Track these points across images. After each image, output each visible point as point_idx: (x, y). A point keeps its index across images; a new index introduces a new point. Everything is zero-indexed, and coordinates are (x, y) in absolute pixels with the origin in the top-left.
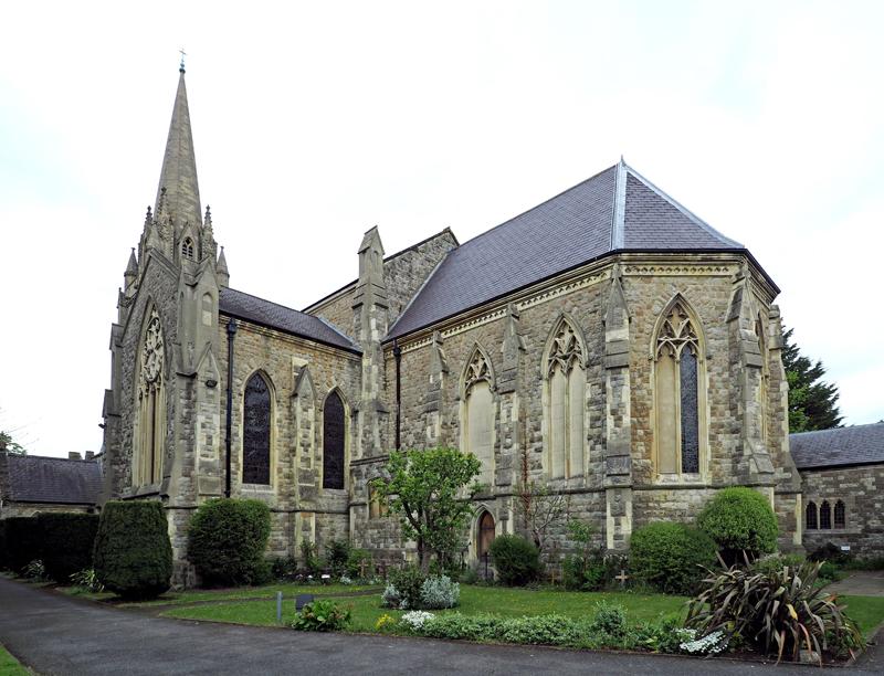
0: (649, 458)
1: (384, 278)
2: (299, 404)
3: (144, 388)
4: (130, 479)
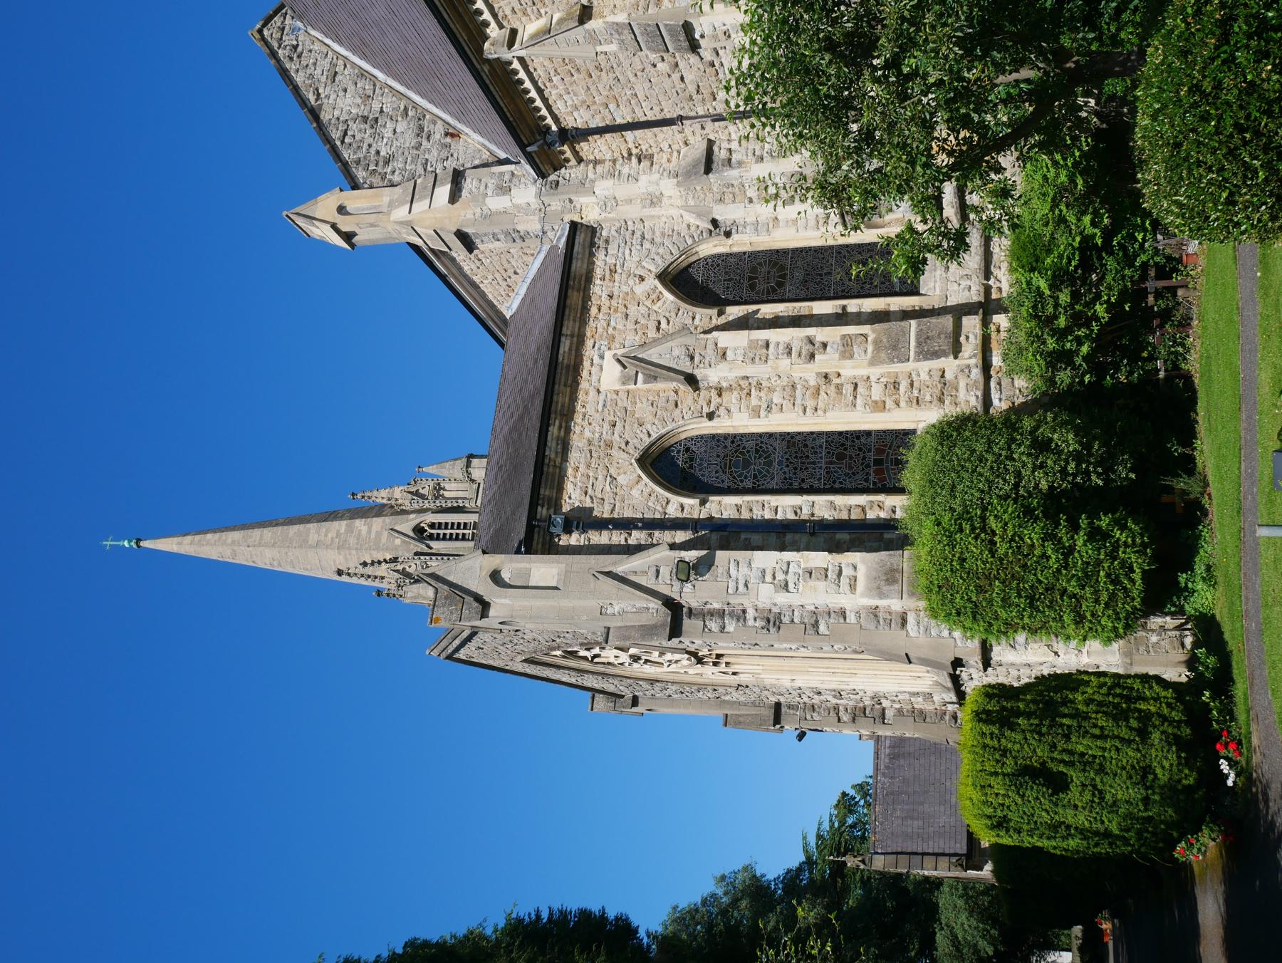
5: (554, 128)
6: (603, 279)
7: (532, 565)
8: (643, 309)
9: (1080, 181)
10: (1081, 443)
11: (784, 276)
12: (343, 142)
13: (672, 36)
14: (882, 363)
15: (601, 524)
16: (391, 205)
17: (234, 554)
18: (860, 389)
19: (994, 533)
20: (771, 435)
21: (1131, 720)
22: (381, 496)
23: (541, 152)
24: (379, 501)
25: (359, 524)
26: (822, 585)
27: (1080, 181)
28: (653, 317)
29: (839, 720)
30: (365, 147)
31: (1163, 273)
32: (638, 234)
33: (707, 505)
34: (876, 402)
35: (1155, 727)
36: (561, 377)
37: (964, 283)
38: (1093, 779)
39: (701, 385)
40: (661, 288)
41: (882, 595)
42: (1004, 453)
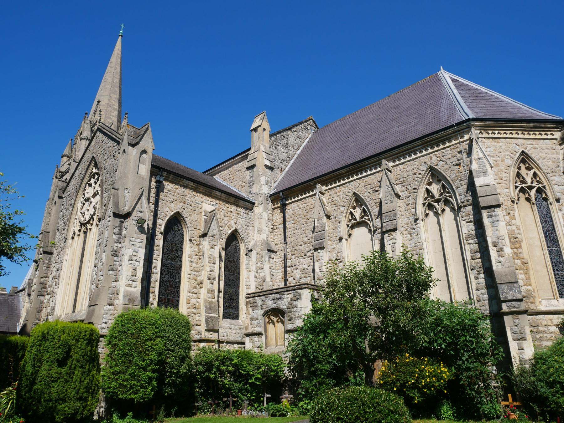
0: (530, 285)
1: (270, 147)
2: (207, 242)
3: (78, 228)
4: (53, 309)
5: (287, 202)
6: (237, 210)
8: (226, 222)
9: (272, 374)
10: (182, 375)
11: (231, 272)
12: (282, 135)
13: (320, 243)
14: (205, 303)
15: (158, 194)
16: (264, 146)
17: (111, 67)
18: (195, 295)
19: (154, 340)
20: (181, 261)
21: (86, 394)
22: (124, 123)
23: (279, 197)
24: (123, 122)
25: (116, 113)
26: (130, 274)
27: (272, 374)
28: (224, 225)
29: (42, 277)
30: (280, 142)
31: (234, 403)
32: (249, 224)
33: (160, 235)
34: (190, 300)
35: (82, 404)
36: (208, 190)
37: (225, 334)
38: (63, 378)
39: (202, 239)
40: (233, 229)
41: (124, 296)
42: (182, 345)
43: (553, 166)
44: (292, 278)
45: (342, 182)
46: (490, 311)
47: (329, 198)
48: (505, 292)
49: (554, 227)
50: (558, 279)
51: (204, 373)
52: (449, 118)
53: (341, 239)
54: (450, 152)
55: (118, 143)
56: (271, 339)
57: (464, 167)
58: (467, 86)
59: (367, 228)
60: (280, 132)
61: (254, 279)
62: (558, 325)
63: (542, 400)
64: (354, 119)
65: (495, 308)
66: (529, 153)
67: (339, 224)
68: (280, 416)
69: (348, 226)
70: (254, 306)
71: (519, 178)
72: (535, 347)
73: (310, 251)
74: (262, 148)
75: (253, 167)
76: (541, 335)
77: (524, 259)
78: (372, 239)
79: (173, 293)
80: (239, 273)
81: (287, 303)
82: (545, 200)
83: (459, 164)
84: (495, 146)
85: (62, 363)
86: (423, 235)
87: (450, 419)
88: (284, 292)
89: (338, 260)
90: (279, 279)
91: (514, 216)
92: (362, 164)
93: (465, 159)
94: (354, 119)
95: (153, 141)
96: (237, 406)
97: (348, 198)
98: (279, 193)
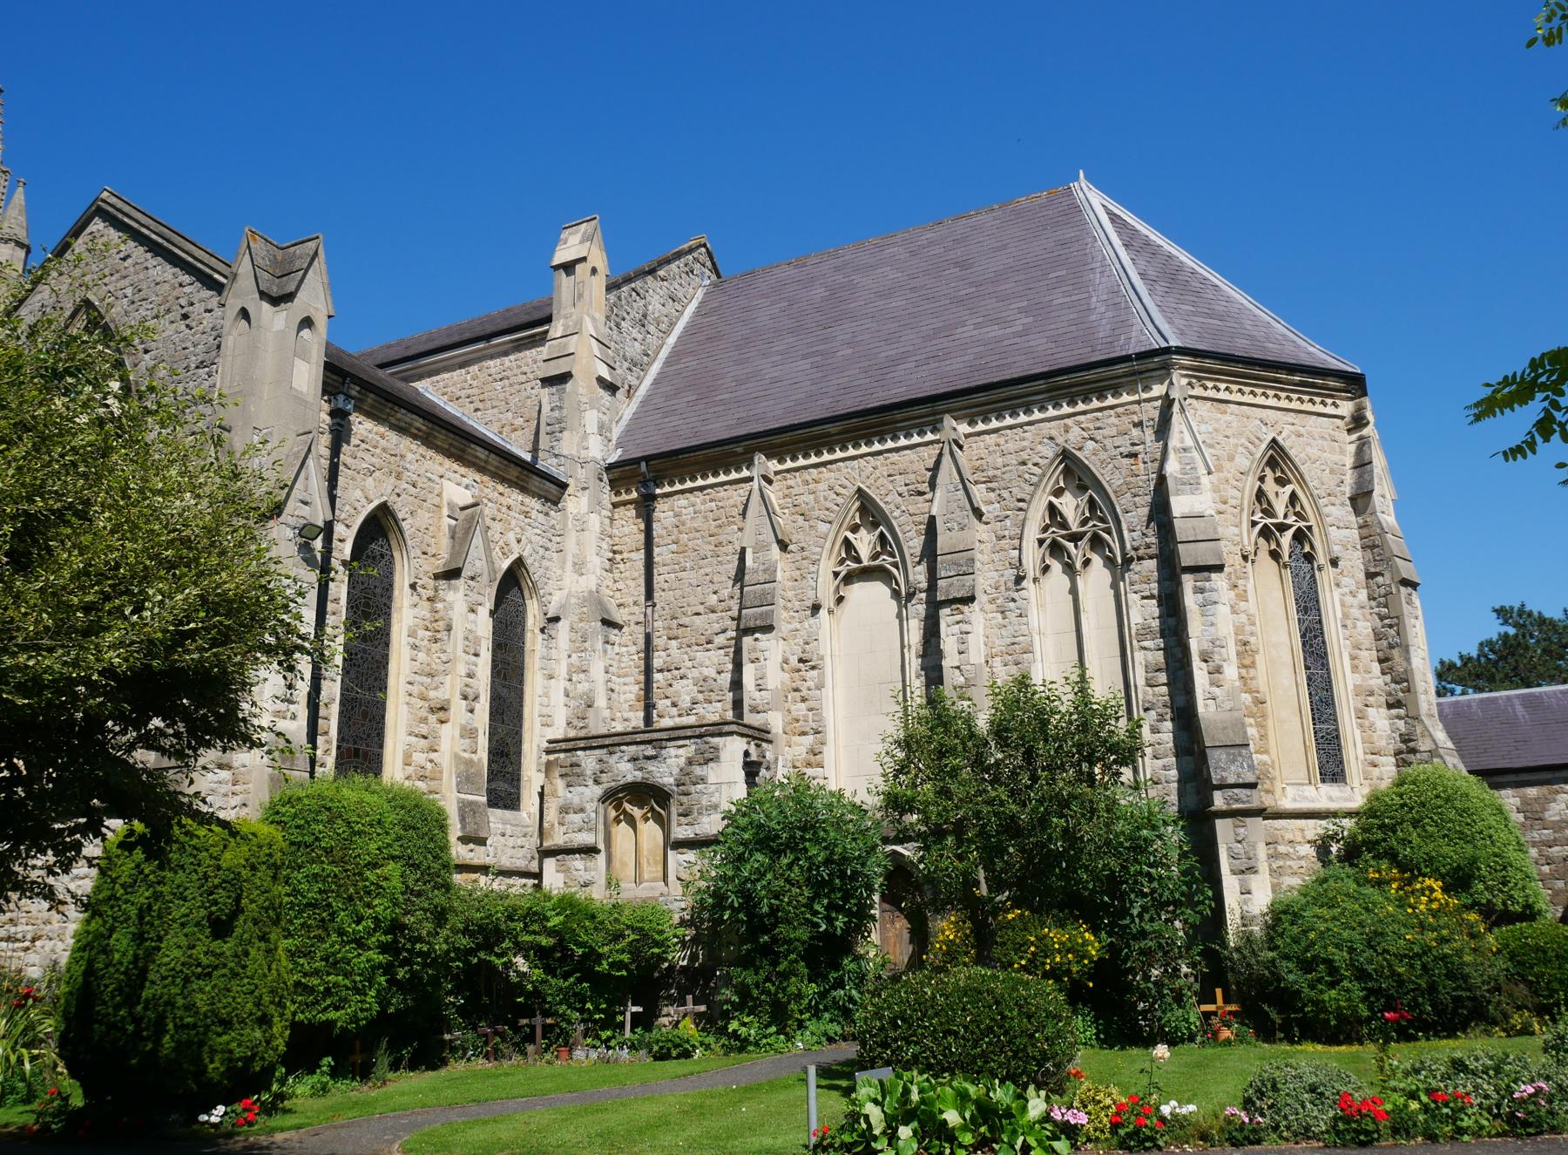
0: (1266, 752)
5: (658, 491)
7: (314, 367)
12: (633, 290)
13: (761, 614)
15: (335, 450)
16: (594, 319)
18: (422, 740)
20: (387, 645)
32: (549, 545)
34: (411, 756)
38: (225, 966)
39: (442, 583)
43: (1331, 481)
44: (668, 702)
45: (826, 457)
46: (1180, 806)
47: (786, 496)
48: (1222, 767)
49: (1320, 622)
50: (1320, 741)
51: (472, 952)
52: (1117, 332)
53: (816, 608)
54: (1113, 420)
55: (218, 288)
56: (623, 864)
57: (1145, 463)
58: (1147, 243)
59: (889, 585)
60: (628, 280)
61: (563, 699)
62: (1315, 841)
63: (1286, 998)
64: (837, 269)
65: (1192, 802)
66: (1286, 444)
67: (813, 569)
68: (678, 1057)
69: (836, 574)
70: (572, 775)
71: (1261, 504)
72: (1275, 888)
73: (724, 631)
74: (589, 327)
75: (564, 378)
76: (1281, 863)
77: (1258, 692)
78: (899, 616)
79: (369, 736)
80: (521, 682)
81: (676, 771)
82: (1309, 558)
83: (1134, 455)
84: (1217, 420)
85: (220, 928)
86: (1034, 617)
87: (1092, 1046)
88: (668, 740)
89: (806, 661)
90: (626, 701)
91: (1245, 591)
92: (888, 417)
93: (1149, 444)
94: (837, 269)
95: (329, 292)
96: (559, 1039)
97: (840, 500)
98: (637, 461)
